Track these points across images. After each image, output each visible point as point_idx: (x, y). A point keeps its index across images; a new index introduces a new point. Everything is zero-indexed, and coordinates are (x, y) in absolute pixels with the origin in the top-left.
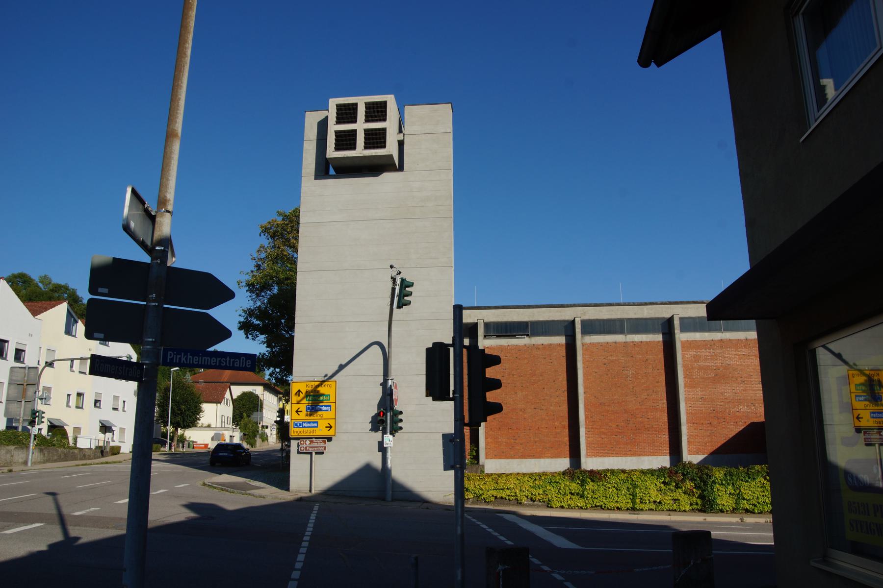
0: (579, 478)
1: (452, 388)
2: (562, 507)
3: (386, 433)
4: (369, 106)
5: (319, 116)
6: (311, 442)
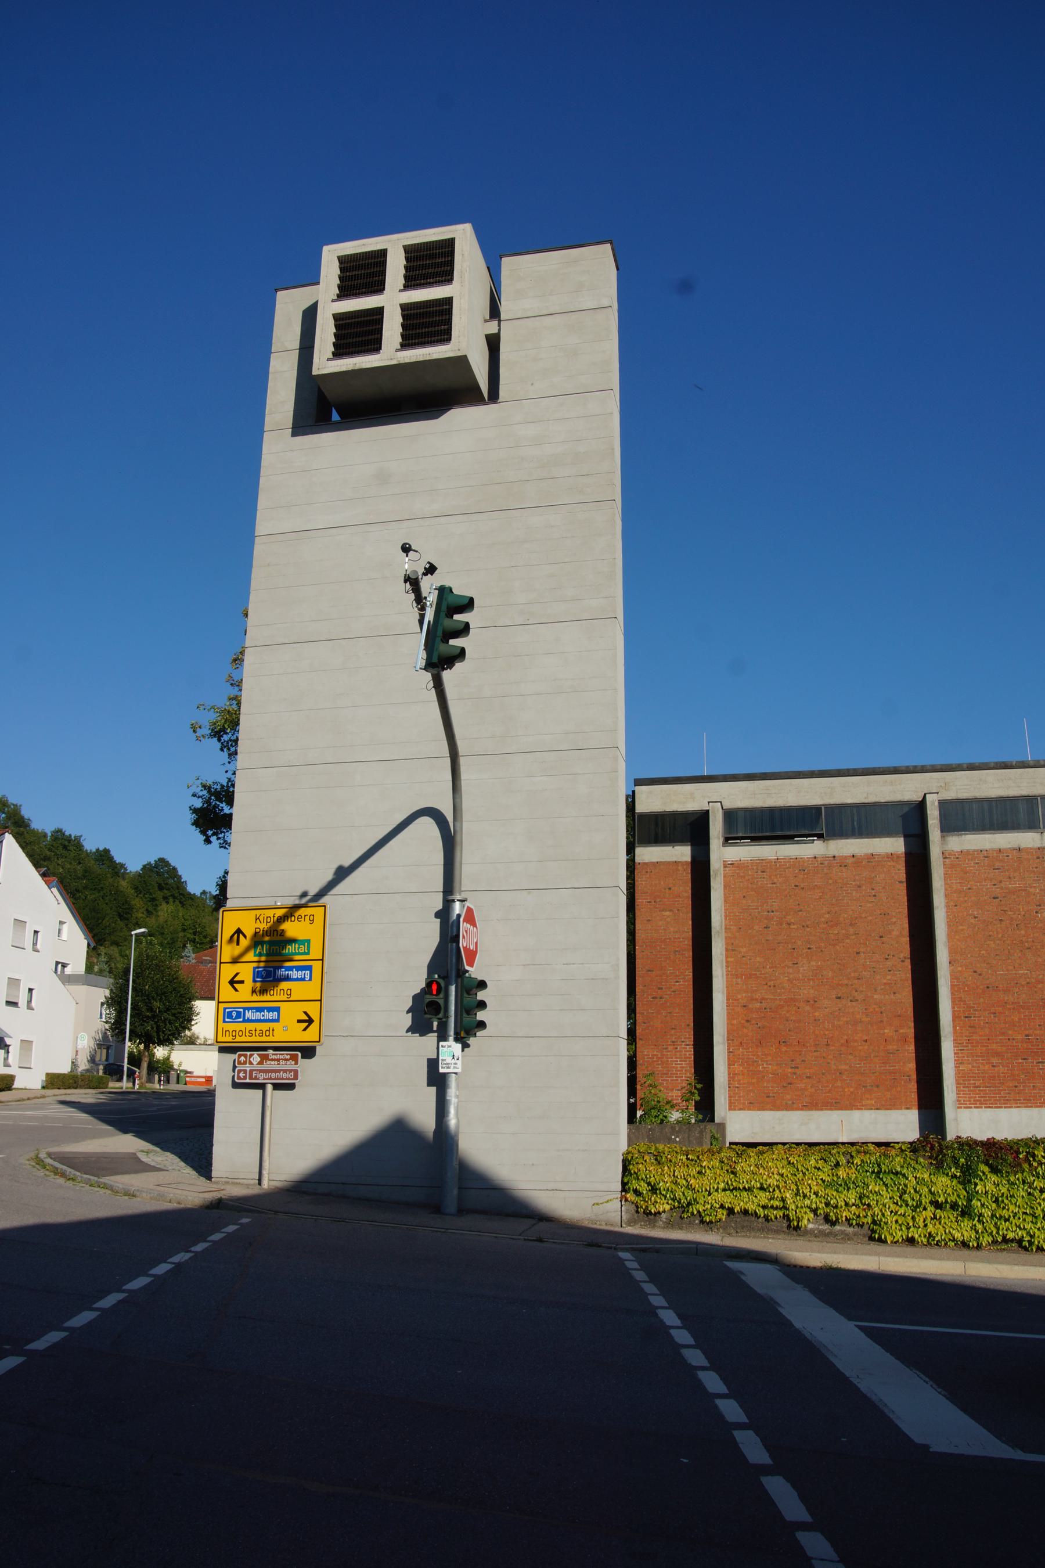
0: (956, 1162)
2: (911, 1241)
6: (264, 1058)
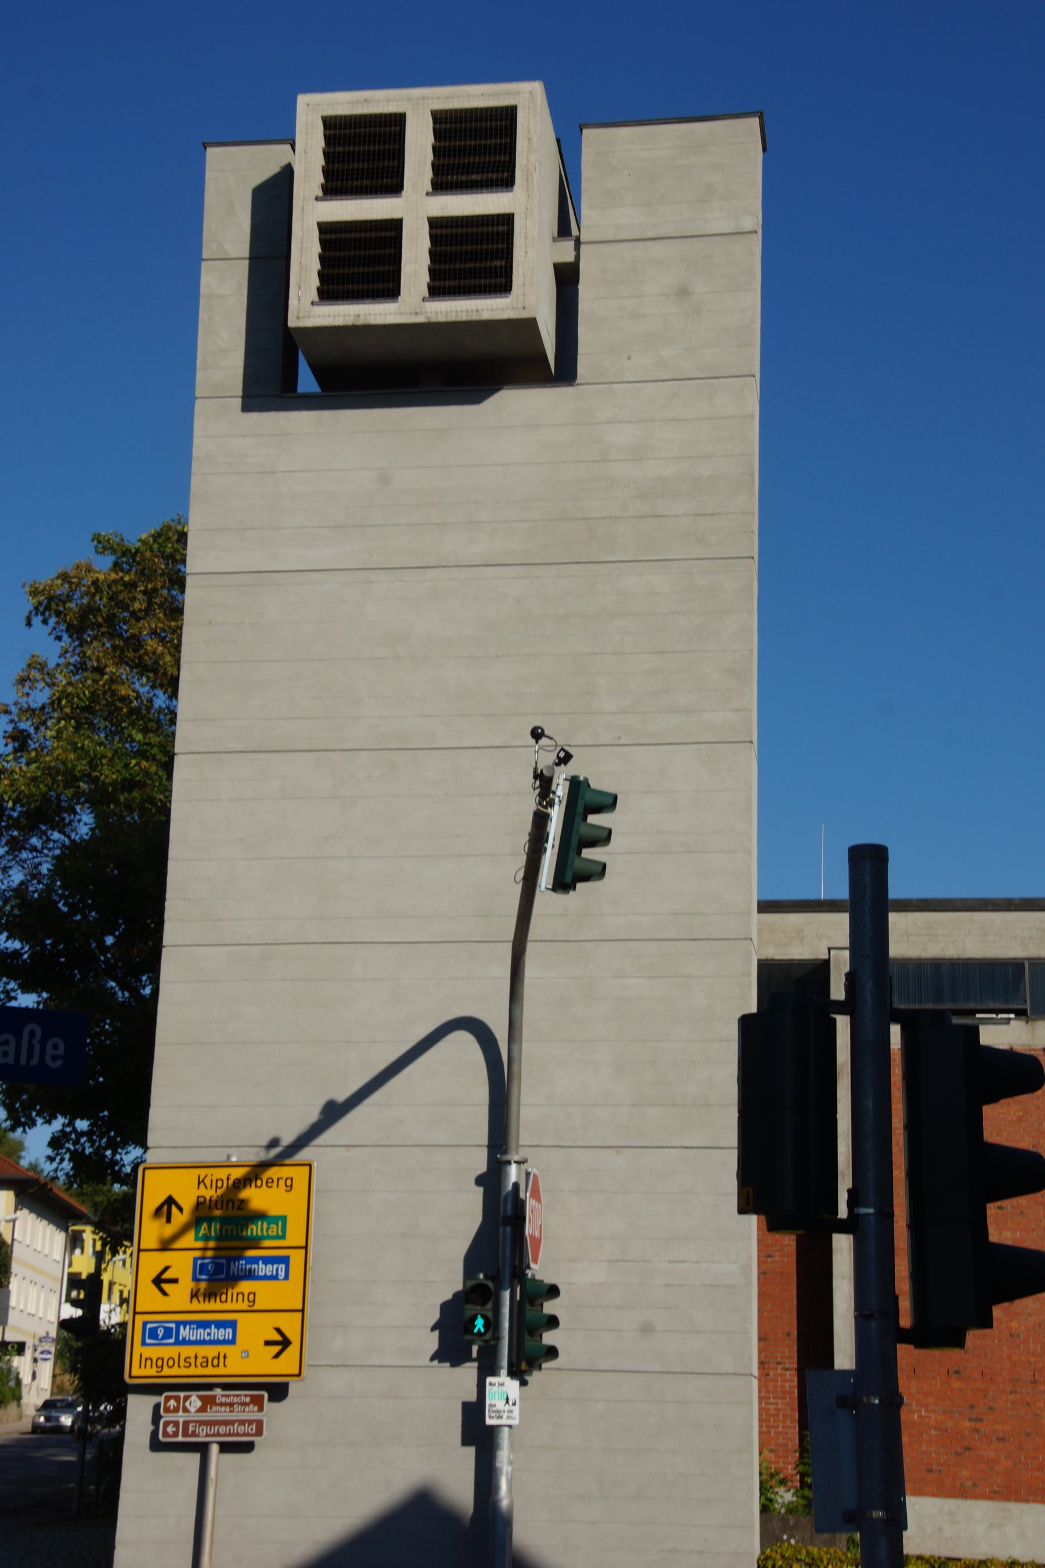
1: (845, 1183)
3: (494, 1373)
4: (446, 124)
5: (260, 162)
6: (208, 1403)
